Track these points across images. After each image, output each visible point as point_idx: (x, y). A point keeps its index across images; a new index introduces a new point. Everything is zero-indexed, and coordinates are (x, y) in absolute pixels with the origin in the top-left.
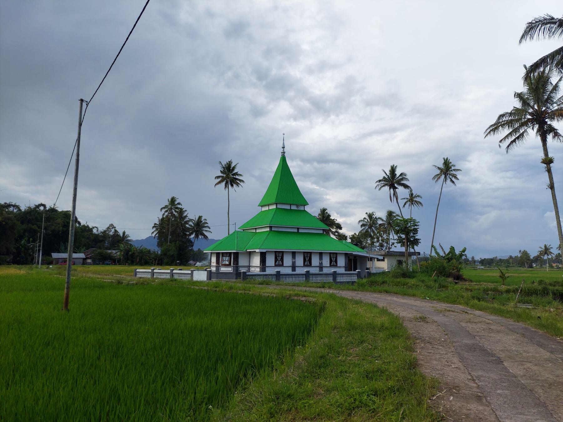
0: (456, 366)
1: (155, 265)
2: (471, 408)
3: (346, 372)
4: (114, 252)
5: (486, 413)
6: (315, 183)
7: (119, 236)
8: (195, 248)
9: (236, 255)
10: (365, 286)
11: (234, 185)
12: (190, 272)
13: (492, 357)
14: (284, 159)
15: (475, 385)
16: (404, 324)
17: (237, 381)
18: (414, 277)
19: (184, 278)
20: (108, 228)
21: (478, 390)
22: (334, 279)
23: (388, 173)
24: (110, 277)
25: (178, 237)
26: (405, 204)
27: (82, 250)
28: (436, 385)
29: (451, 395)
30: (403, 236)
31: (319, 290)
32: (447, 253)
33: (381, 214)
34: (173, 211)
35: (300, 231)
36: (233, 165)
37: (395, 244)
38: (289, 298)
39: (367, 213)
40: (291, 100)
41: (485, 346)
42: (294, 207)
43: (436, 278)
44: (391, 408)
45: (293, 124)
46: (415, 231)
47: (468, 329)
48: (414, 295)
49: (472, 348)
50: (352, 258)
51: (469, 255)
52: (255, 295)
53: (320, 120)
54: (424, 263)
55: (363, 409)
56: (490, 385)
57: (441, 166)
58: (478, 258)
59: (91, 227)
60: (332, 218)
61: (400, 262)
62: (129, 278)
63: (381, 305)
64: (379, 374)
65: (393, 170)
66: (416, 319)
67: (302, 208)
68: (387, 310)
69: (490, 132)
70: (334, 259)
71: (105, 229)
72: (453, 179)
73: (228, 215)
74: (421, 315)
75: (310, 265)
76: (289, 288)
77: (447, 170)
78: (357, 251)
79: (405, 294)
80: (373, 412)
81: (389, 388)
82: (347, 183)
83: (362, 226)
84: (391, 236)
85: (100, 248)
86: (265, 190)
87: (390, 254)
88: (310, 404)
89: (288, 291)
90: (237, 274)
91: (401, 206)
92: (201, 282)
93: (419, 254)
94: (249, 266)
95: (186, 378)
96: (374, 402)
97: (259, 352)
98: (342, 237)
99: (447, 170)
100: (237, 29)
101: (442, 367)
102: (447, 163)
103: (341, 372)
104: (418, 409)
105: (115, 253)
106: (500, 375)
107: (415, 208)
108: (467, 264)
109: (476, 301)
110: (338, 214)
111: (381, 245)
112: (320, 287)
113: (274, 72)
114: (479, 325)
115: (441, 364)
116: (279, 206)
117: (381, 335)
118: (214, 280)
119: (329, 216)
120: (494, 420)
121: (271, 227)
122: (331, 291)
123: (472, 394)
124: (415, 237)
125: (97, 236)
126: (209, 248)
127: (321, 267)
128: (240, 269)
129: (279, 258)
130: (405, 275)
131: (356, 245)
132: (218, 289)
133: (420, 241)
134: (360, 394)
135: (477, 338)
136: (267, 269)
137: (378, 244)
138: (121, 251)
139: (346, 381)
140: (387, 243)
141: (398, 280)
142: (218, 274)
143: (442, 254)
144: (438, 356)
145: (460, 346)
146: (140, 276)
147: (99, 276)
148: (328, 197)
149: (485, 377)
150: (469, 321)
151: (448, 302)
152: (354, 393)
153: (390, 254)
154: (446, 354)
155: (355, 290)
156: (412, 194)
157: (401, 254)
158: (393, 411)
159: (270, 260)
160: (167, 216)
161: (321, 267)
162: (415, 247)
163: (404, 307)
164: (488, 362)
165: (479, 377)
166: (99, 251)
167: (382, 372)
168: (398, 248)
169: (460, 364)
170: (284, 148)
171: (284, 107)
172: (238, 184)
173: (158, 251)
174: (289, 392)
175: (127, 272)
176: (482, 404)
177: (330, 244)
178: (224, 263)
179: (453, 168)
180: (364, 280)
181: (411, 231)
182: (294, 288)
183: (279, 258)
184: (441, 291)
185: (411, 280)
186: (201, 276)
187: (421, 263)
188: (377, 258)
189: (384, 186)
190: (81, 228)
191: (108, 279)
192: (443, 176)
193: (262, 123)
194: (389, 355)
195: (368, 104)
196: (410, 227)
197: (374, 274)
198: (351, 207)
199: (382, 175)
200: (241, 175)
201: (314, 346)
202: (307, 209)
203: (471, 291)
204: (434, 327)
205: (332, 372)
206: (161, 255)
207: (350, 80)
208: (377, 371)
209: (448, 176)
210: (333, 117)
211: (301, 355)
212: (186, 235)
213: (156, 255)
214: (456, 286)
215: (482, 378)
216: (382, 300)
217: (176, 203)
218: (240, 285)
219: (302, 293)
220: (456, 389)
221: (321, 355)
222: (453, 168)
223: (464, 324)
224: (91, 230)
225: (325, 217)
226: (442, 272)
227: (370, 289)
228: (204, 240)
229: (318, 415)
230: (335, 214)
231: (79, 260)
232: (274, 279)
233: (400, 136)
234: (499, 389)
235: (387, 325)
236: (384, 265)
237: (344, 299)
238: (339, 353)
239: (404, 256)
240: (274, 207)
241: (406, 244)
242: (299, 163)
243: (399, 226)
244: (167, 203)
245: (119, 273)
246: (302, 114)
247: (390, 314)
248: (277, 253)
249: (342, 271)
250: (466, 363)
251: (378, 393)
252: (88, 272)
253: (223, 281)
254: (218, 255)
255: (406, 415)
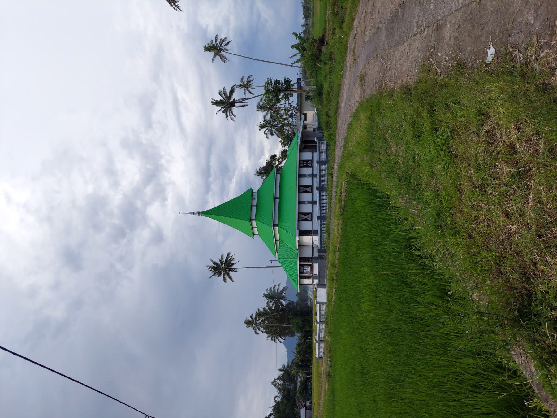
0: (407, 48)
1: (311, 339)
2: (448, 35)
3: (414, 157)
4: (299, 379)
5: (453, 21)
6: (230, 180)
7: (283, 375)
8: (295, 299)
9: (302, 259)
10: (331, 134)
11: (233, 262)
12: (318, 305)
13: (398, 12)
14: (206, 213)
15: (426, 31)
16: (368, 97)
17: (423, 266)
18: (322, 85)
19: (324, 311)
20: (275, 386)
21: (431, 28)
22: (324, 163)
23: (219, 108)
24: (323, 384)
25: (283, 317)
26: (250, 92)
27: (297, 410)
28: (427, 69)
29: (436, 54)
30: (282, 94)
31: (335, 179)
32: (297, 52)
33: (260, 117)
34: (258, 322)
35: (278, 196)
36: (213, 265)
37: (290, 102)
38: (343, 209)
39: (260, 130)
40: (146, 204)
41: (388, 18)
42: (255, 203)
43: (322, 63)
44: (449, 115)
45: (170, 202)
46: (277, 82)
47: (372, 35)
48: (340, 86)
49: (390, 33)
50: (304, 145)
51: (300, 30)
52: (341, 242)
53: (166, 174)
54: (308, 75)
55: (451, 142)
56: (426, 15)
57: (212, 54)
58: (302, 21)
59: (275, 403)
60: (265, 164)
61: (308, 98)
62: (325, 366)
63: (349, 119)
64: (415, 124)
65: (217, 103)
66: (362, 85)
67: (255, 195)
68: (354, 114)
69: (176, 6)
70: (305, 163)
71: (277, 390)
72: (225, 43)
73: (262, 268)
74: (359, 80)
75: (311, 187)
76: (333, 205)
77: (216, 48)
78: (297, 140)
79: (339, 95)
80: (453, 133)
81: (430, 115)
82: (230, 149)
83: (272, 134)
84: (282, 106)
85: (296, 393)
86: (238, 232)
87: (300, 108)
88: (446, 195)
89: (336, 209)
90: (320, 258)
91: (252, 96)
92: (328, 294)
93: (299, 79)
94: (313, 246)
95: (421, 314)
96: (444, 131)
97: (395, 240)
98: (284, 154)
99: (216, 48)
100: (72, 258)
101: (409, 61)
102: (209, 48)
103: (414, 162)
104: (450, 88)
105: (300, 379)
106: (416, 5)
107: (254, 83)
108: (309, 32)
109: (345, 25)
110: (261, 158)
111: (291, 116)
112: (332, 177)
113: (116, 221)
114: (368, 23)
115: (405, 63)
116: (253, 217)
117: (378, 120)
118: (326, 281)
119: (264, 168)
120: (460, 14)
121: (275, 225)
122: (336, 167)
123: (435, 34)
124: (282, 83)
125: (284, 397)
126: (295, 287)
127: (313, 176)
128: (315, 255)
129: (305, 217)
130: (320, 93)
131: (291, 141)
132: (335, 278)
133: (287, 78)
134: (436, 145)
135: (380, 25)
136: (315, 229)
137: (290, 120)
138: (298, 372)
139: (423, 158)
140: (289, 110)
141: (325, 99)
142: (320, 276)
143: (299, 56)
144: (398, 65)
145: (388, 43)
146: (322, 353)
147: (323, 394)
148: (244, 168)
149: (418, 20)
150: (364, 32)
151: (346, 53)
152: (435, 151)
153: (300, 108)
154: (396, 57)
155: (335, 143)
156: (240, 85)
157: (300, 96)
158: (452, 113)
159: (307, 226)
160: (264, 328)
161: (313, 176)
162: (292, 83)
163: (351, 97)
164: (403, 16)
165: (418, 26)
166: (298, 394)
167: (414, 122)
168: (294, 99)
169: (406, 44)
170: (194, 213)
171: (154, 211)
172: (232, 259)
173: (298, 335)
174: (435, 215)
175: (319, 367)
176: (445, 24)
177: (290, 166)
178: (309, 271)
179: (214, 43)
180: (326, 134)
181: (276, 87)
182: (333, 203)
183: (305, 217)
184: (335, 59)
185: (325, 86)
186: (322, 294)
187: (308, 76)
188: (304, 120)
189: (232, 113)
190: (276, 413)
191: (325, 386)
192: (222, 53)
193: (169, 232)
194: (397, 114)
195: (149, 126)
196: (272, 88)
197: (319, 124)
198: (254, 146)
199: (222, 115)
200: (222, 256)
201: (389, 187)
202: (256, 189)
203: (334, 29)
204: (370, 68)
205: (414, 171)
206: (302, 332)
207: (125, 144)
208: (414, 127)
209: (223, 48)
210: (163, 162)
211: (399, 200)
212: (282, 309)
213: (302, 337)
214: (330, 43)
215: (419, 23)
216: (344, 117)
217: (251, 319)
218: (331, 256)
219: (338, 195)
220: (430, 50)
221: (397, 181)
222: (214, 43)
223: (367, 39)
224: (278, 403)
225: (265, 171)
226: (316, 57)
227: (333, 129)
228: (287, 291)
229: (456, 187)
230: (261, 160)
231: (308, 414)
232: (325, 222)
233: (181, 94)
234: (430, 6)
235: (368, 114)
236: (311, 114)
237: (343, 155)
238: (396, 163)
239: (301, 94)
240: (254, 223)
241: (289, 92)
242: (210, 195)
243: (272, 99)
244: (251, 328)
245: (319, 374)
246: (160, 193)
247: (357, 110)
248: (300, 219)
249: (316, 155)
250: (405, 38)
251: (434, 126)
252: (319, 406)
253: (327, 273)
254: (301, 278)
255: (456, 100)
